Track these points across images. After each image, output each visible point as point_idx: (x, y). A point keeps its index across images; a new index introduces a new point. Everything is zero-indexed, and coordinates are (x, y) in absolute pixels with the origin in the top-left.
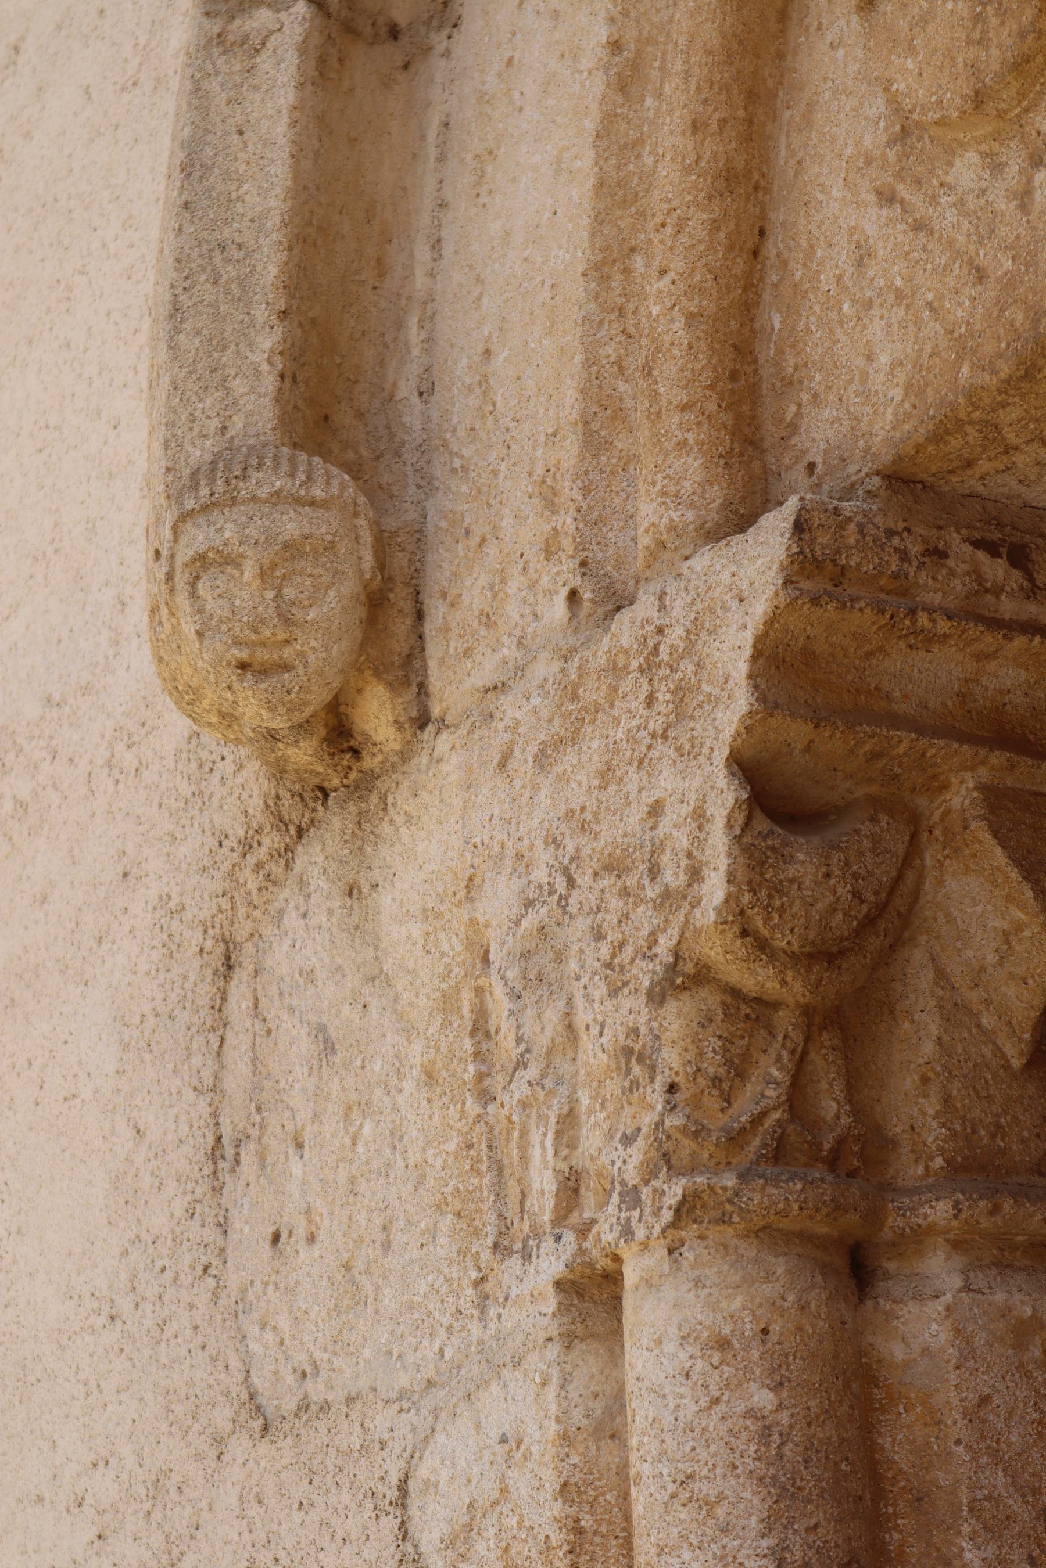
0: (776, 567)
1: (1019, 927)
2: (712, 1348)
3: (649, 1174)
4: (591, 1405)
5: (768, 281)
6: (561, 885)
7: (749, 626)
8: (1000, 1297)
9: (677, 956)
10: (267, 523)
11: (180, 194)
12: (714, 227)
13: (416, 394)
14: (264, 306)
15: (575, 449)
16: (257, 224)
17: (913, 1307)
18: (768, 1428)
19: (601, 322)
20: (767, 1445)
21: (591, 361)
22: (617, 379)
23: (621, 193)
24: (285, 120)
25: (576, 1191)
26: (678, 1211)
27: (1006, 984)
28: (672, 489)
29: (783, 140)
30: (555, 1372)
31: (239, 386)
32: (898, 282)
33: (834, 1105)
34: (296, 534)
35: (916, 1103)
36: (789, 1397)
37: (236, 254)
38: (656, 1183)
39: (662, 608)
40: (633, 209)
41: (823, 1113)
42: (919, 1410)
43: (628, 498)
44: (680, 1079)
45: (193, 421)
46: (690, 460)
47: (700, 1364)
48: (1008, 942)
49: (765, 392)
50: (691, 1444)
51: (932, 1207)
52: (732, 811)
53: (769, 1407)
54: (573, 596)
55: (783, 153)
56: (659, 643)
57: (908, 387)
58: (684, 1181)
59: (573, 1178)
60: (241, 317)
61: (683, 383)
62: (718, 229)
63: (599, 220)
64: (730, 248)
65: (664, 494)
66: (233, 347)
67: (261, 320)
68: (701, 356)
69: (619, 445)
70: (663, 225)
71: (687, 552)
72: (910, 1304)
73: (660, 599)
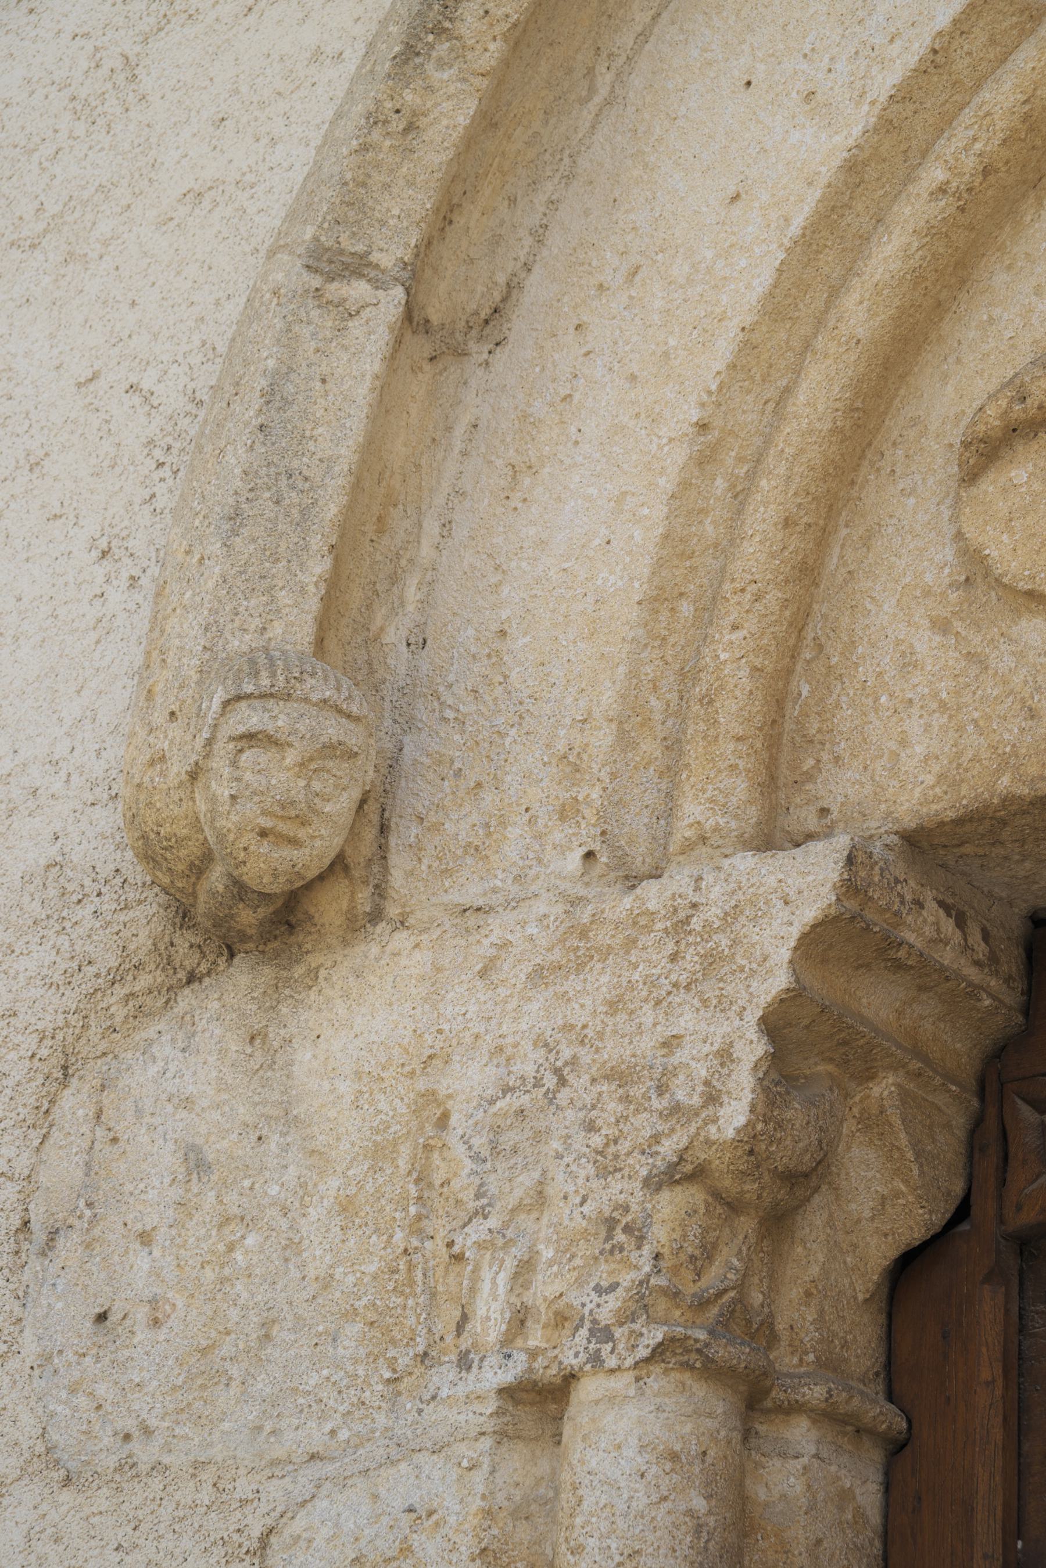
0: (829, 885)
1: (898, 1194)
2: (665, 1458)
3: (625, 1317)
4: (512, 1491)
5: (802, 656)
6: (550, 1081)
7: (796, 924)
8: (833, 1468)
9: (681, 1159)
10: (314, 724)
11: (257, 417)
12: (785, 604)
13: (405, 644)
14: (319, 536)
15: (609, 740)
16: (325, 465)
17: (777, 1462)
18: (700, 1526)
19: (646, 645)
20: (699, 1538)
21: (633, 674)
22: (650, 694)
23: (681, 547)
24: (368, 384)
25: (522, 1322)
26: (654, 1350)
27: (871, 1236)
28: (721, 799)
29: (836, 551)
30: (486, 1461)
31: (284, 598)
32: (944, 695)
33: (761, 1296)
34: (334, 740)
35: (798, 1310)
36: (716, 1507)
37: (300, 484)
38: (636, 1326)
39: (697, 889)
40: (688, 564)
41: (751, 1301)
42: (773, 1540)
43: (645, 791)
44: (666, 1251)
45: (237, 614)
46: (739, 781)
47: (654, 1469)
48: (883, 1205)
49: (784, 741)
50: (641, 1527)
51: (810, 1389)
52: (760, 1059)
53: (703, 1511)
54: (589, 855)
55: (835, 560)
56: (693, 915)
57: (941, 777)
58: (666, 1328)
59: (522, 1312)
60: (296, 540)
61: (740, 720)
62: (786, 607)
63: (660, 563)
64: (791, 624)
65: (711, 800)
66: (284, 563)
67: (315, 548)
68: (757, 703)
69: (644, 747)
70: (743, 590)
71: (727, 852)
72: (775, 1459)
73: (696, 881)
